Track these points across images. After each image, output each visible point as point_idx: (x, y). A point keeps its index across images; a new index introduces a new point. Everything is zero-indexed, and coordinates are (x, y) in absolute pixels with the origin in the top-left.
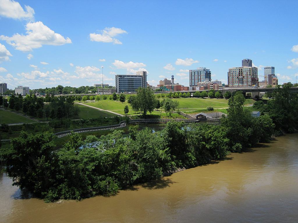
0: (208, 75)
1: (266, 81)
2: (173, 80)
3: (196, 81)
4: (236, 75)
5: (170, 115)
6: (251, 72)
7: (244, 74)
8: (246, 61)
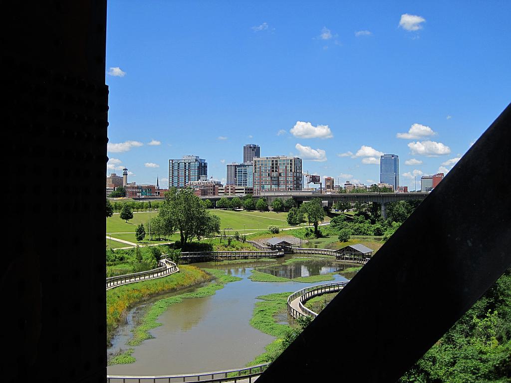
0: (202, 169)
1: (189, 180)
2: (125, 176)
3: (182, 179)
4: (266, 171)
5: (229, 244)
6: (293, 167)
7: (281, 169)
8: (250, 147)
